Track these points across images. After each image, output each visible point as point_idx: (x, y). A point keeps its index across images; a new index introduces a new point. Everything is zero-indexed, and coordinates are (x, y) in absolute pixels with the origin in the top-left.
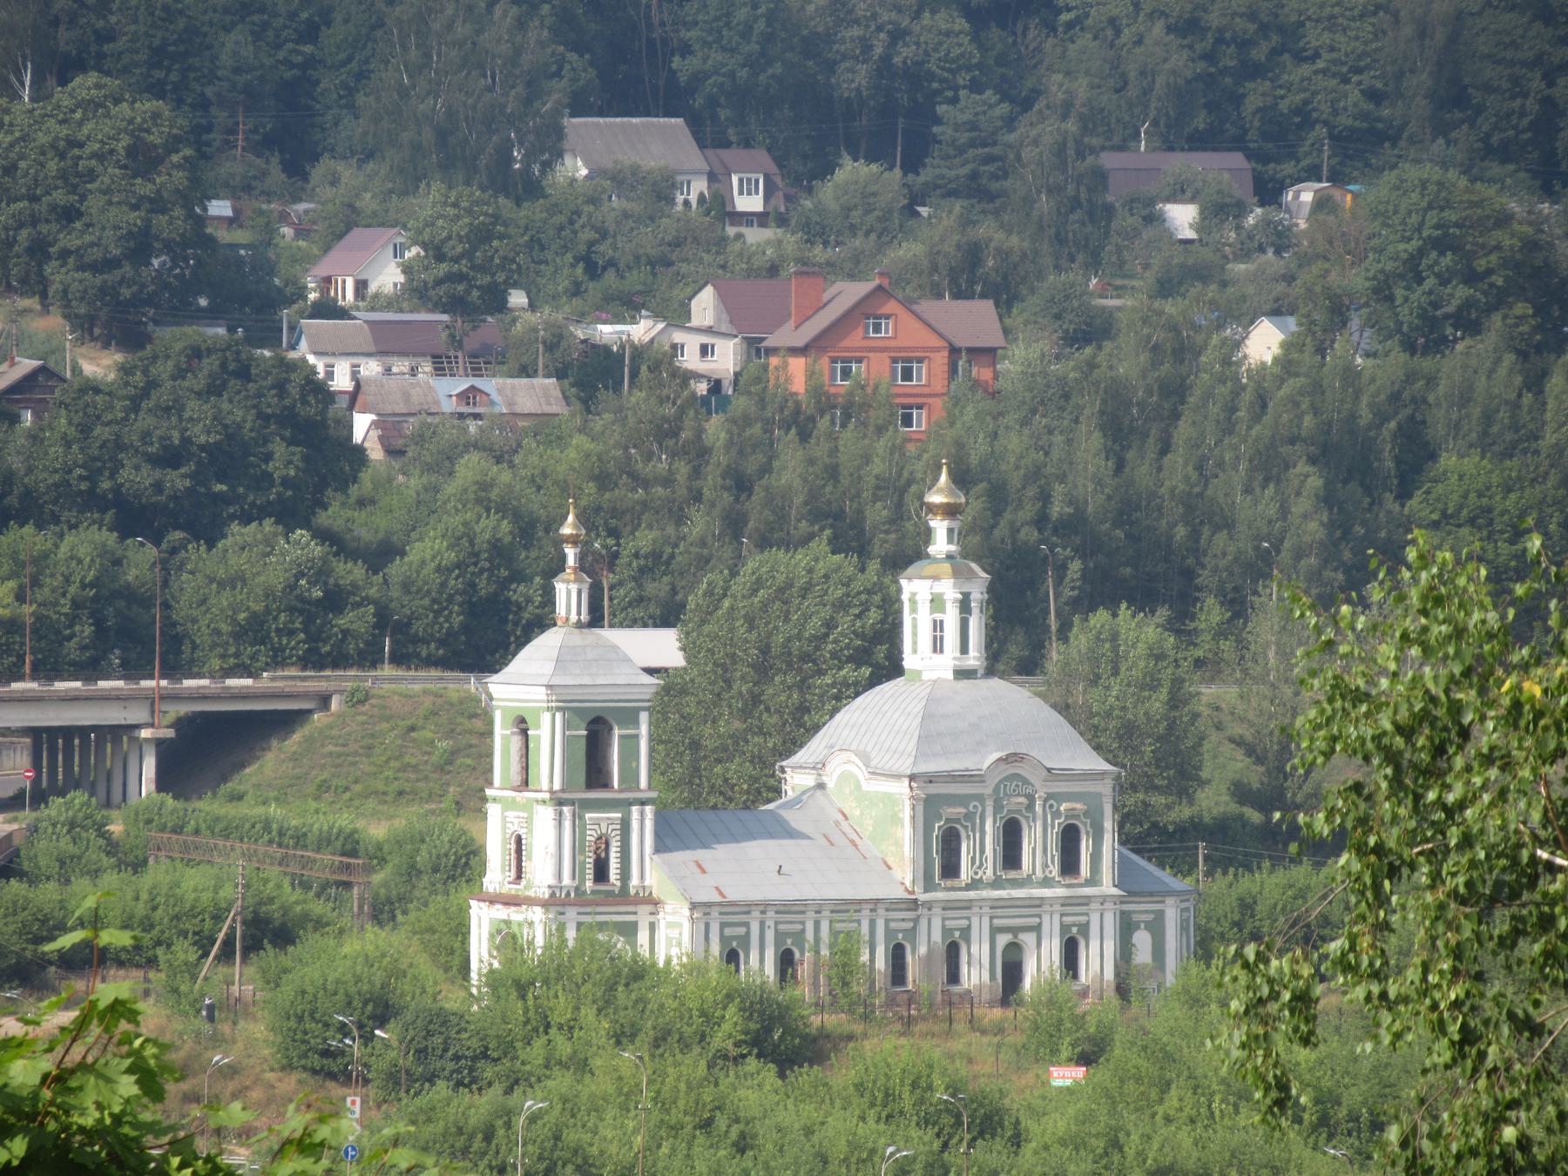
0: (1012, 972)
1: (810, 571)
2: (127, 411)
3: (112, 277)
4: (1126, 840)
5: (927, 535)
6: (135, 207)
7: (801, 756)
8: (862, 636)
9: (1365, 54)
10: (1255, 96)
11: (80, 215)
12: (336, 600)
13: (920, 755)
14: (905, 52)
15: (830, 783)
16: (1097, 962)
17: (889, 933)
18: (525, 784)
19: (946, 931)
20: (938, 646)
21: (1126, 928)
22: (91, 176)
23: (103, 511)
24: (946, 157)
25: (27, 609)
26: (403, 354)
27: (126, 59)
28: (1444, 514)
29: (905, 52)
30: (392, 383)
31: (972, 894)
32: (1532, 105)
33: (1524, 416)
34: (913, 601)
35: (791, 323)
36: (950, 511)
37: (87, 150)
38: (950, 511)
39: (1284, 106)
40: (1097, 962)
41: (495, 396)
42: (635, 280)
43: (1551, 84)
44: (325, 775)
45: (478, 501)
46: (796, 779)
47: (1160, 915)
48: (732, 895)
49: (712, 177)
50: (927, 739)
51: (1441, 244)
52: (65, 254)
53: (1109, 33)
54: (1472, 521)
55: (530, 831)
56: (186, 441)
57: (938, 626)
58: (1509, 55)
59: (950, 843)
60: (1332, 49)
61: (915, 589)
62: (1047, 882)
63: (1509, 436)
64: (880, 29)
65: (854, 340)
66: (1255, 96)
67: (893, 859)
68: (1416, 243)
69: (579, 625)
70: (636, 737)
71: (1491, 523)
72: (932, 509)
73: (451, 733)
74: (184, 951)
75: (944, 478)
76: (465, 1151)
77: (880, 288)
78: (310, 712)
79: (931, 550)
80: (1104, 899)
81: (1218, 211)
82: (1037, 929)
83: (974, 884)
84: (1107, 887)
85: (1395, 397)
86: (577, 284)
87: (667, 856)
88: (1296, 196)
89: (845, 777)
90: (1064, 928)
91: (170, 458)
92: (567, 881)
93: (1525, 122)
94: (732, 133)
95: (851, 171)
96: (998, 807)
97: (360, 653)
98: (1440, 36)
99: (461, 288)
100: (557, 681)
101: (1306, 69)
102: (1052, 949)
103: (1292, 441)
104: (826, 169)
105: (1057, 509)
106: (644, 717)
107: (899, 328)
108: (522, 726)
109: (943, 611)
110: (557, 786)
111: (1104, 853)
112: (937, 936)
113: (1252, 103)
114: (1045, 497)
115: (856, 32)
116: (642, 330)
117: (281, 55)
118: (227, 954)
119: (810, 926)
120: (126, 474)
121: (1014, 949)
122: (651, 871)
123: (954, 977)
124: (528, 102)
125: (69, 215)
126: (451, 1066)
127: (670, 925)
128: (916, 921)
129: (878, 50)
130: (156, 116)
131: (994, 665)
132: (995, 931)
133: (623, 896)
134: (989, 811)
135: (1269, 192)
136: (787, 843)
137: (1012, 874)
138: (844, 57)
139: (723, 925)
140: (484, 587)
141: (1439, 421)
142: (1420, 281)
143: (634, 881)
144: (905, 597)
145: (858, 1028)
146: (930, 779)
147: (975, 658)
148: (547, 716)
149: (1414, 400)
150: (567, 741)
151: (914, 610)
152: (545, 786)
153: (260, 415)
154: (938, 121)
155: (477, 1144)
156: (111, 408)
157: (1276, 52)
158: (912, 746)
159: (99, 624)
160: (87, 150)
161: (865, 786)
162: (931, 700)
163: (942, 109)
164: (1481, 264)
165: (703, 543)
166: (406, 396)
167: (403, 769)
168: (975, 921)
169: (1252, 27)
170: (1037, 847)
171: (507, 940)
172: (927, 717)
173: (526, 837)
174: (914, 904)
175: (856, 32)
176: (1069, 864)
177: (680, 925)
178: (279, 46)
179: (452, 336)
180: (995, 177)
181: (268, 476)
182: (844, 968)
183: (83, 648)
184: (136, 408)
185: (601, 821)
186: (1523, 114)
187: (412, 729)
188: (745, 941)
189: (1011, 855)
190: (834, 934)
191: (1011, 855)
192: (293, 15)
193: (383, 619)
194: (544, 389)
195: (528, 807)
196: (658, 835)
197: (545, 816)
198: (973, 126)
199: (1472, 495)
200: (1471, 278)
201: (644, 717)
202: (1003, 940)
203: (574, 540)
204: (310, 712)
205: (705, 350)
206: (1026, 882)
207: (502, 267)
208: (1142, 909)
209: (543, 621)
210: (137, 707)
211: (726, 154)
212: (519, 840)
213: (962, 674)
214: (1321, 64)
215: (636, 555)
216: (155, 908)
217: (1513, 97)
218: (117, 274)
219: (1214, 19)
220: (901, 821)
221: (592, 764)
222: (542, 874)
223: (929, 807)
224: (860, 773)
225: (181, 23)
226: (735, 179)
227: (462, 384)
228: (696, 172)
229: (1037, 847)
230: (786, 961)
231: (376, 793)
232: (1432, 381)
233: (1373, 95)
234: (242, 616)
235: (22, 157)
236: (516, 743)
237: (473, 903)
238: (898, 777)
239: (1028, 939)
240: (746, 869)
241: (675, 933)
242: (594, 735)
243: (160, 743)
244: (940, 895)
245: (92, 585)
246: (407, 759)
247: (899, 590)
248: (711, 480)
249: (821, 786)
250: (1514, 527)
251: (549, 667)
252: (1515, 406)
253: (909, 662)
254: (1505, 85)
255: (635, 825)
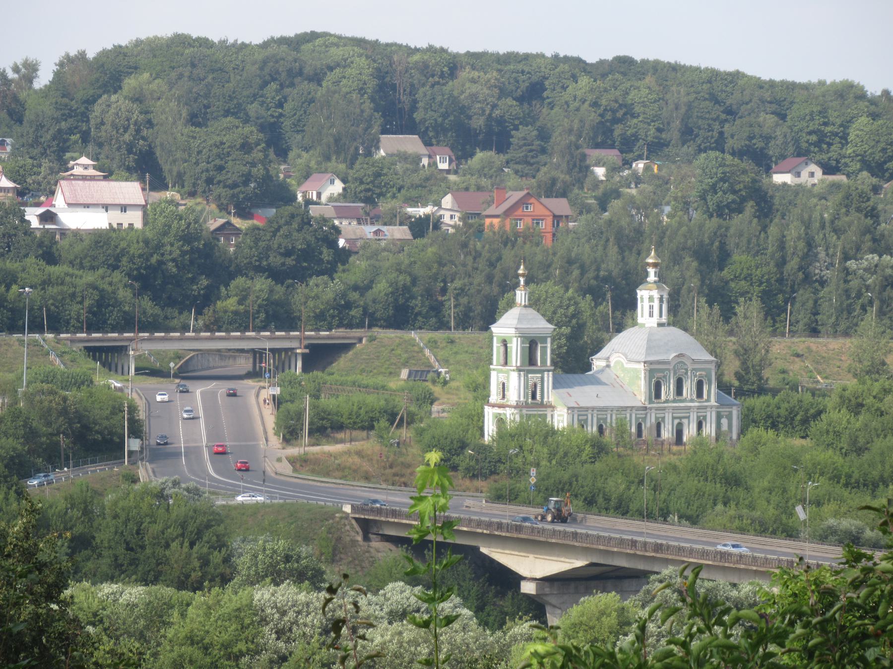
0: (679, 433)
1: (546, 292)
2: (272, 237)
3: (236, 190)
4: (718, 387)
5: (647, 274)
6: (245, 165)
7: (598, 355)
8: (566, 316)
9: (656, 116)
10: (618, 130)
11: (224, 168)
12: (349, 305)
13: (647, 354)
14: (497, 112)
15: (612, 365)
16: (710, 430)
17: (637, 419)
18: (506, 363)
19: (657, 418)
20: (651, 315)
21: (719, 417)
22: (229, 154)
23: (264, 273)
24: (515, 150)
25: (242, 307)
26: (346, 218)
27: (215, 114)
28: (736, 277)
29: (497, 112)
30: (350, 228)
31: (666, 405)
32: (716, 134)
33: (761, 241)
34: (642, 298)
35: (494, 206)
36: (655, 265)
37: (226, 145)
38: (655, 265)
39: (629, 133)
40: (710, 430)
41: (386, 233)
42: (414, 193)
43: (722, 127)
44: (363, 366)
45: (397, 270)
46: (598, 362)
47: (731, 413)
48: (582, 404)
49: (430, 157)
50: (649, 349)
51: (723, 180)
52: (219, 182)
53: (566, 106)
54: (745, 279)
55: (508, 381)
56: (293, 247)
57: (651, 307)
58: (707, 116)
59: (658, 386)
60: (644, 113)
61: (642, 294)
62: (692, 401)
63: (756, 248)
64: (488, 104)
65: (519, 212)
66: (618, 130)
67: (639, 393)
68: (715, 179)
69: (525, 306)
70: (546, 347)
71: (751, 279)
72: (648, 264)
73: (406, 352)
74: (383, 423)
75: (653, 253)
76: (562, 490)
77: (528, 193)
78: (355, 344)
79: (648, 279)
80: (712, 407)
81: (612, 170)
82: (688, 417)
83: (667, 401)
84: (713, 402)
85: (715, 234)
86: (394, 194)
87: (561, 391)
88: (637, 165)
89: (617, 362)
90: (698, 417)
91: (288, 254)
92: (522, 399)
93: (713, 140)
94: (434, 141)
95: (480, 155)
96: (675, 374)
97: (357, 324)
98: (683, 110)
99: (370, 194)
100: (519, 326)
101: (635, 121)
102: (694, 427)
103: (683, 249)
104: (472, 155)
105: (602, 273)
106: (549, 340)
107: (535, 208)
108: (505, 343)
109: (653, 301)
110: (519, 364)
111: (711, 391)
112: (653, 420)
113: (617, 133)
114: (598, 269)
115: (479, 105)
116: (428, 210)
117: (269, 113)
118: (400, 425)
119: (628, 416)
120: (271, 259)
121: (680, 425)
122: (551, 396)
123: (659, 435)
124: (366, 130)
125: (220, 169)
126: (487, 465)
127: (559, 415)
128: (646, 414)
129: (487, 112)
130: (252, 132)
131: (672, 323)
132: (674, 418)
133: (542, 405)
134: (672, 375)
135: (627, 164)
136: (600, 387)
137: (680, 398)
138: (475, 114)
139: (579, 415)
140: (401, 301)
141: (731, 243)
142: (716, 193)
143: (545, 399)
144: (639, 297)
145: (629, 452)
146: (651, 363)
147: (664, 319)
148: (515, 339)
149: (721, 235)
150: (523, 348)
151: (642, 301)
152: (514, 364)
153: (316, 238)
154: (512, 137)
155: (566, 487)
156: (265, 235)
157: (625, 114)
158: (644, 351)
159: (267, 313)
160: (226, 145)
161: (626, 366)
162: (650, 334)
163: (513, 132)
164: (737, 187)
165: (479, 285)
166: (355, 233)
167: (392, 364)
168: (667, 415)
169: (617, 105)
170: (689, 388)
171: (500, 421)
172: (649, 340)
173: (507, 384)
174: (645, 408)
175: (479, 105)
176: (700, 394)
177: (563, 415)
178: (268, 110)
179: (365, 212)
180: (533, 157)
181: (322, 260)
182: (621, 430)
183: (262, 321)
184: (274, 235)
185: (534, 377)
186: (712, 137)
187: (393, 350)
188: (586, 421)
189: (679, 391)
190: (617, 419)
191: (679, 391)
192: (273, 98)
193: (365, 312)
194: (404, 230)
195: (507, 372)
196: (553, 383)
197: (514, 376)
198: (525, 139)
199: (745, 270)
200: (734, 192)
201: (549, 340)
202: (676, 421)
203: (523, 275)
204: (355, 344)
205: (452, 217)
206: (684, 401)
207: (385, 186)
208: (724, 410)
209: (511, 304)
210: (294, 341)
211: (434, 148)
212: (504, 384)
213: (660, 325)
214: (640, 119)
215: (455, 289)
216: (360, 408)
217: (709, 131)
218: (238, 189)
219: (604, 102)
220: (640, 379)
221: (530, 358)
222: (513, 396)
223: (651, 373)
224: (623, 360)
225: (235, 101)
226: (438, 157)
227: (375, 228)
228: (425, 155)
229: (689, 388)
230: (601, 429)
231: (382, 373)
232: (727, 229)
233: (659, 130)
234: (318, 311)
235: (204, 148)
236: (502, 349)
237: (486, 407)
238: (639, 362)
239: (685, 421)
240: (585, 395)
241: (561, 418)
242: (531, 344)
243: (303, 355)
244: (655, 405)
245: (266, 300)
246: (392, 361)
247: (636, 294)
248: (482, 264)
249: (608, 366)
250: (760, 281)
251: (515, 322)
252: (758, 237)
253: (640, 320)
254: (706, 127)
255: (546, 379)
